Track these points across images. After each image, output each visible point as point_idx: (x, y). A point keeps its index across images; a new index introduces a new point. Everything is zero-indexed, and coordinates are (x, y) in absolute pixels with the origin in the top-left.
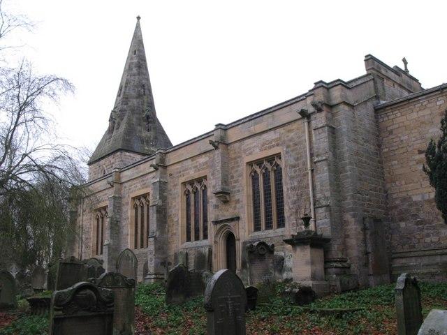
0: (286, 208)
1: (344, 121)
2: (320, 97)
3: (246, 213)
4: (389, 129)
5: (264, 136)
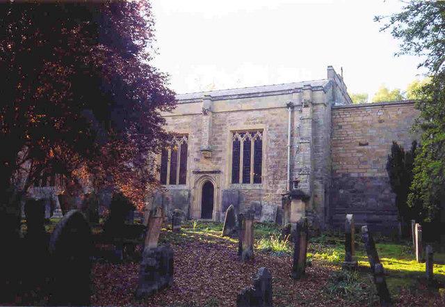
0: (264, 156)
1: (322, 117)
2: (307, 95)
3: (227, 169)
4: (339, 124)
5: (250, 113)
